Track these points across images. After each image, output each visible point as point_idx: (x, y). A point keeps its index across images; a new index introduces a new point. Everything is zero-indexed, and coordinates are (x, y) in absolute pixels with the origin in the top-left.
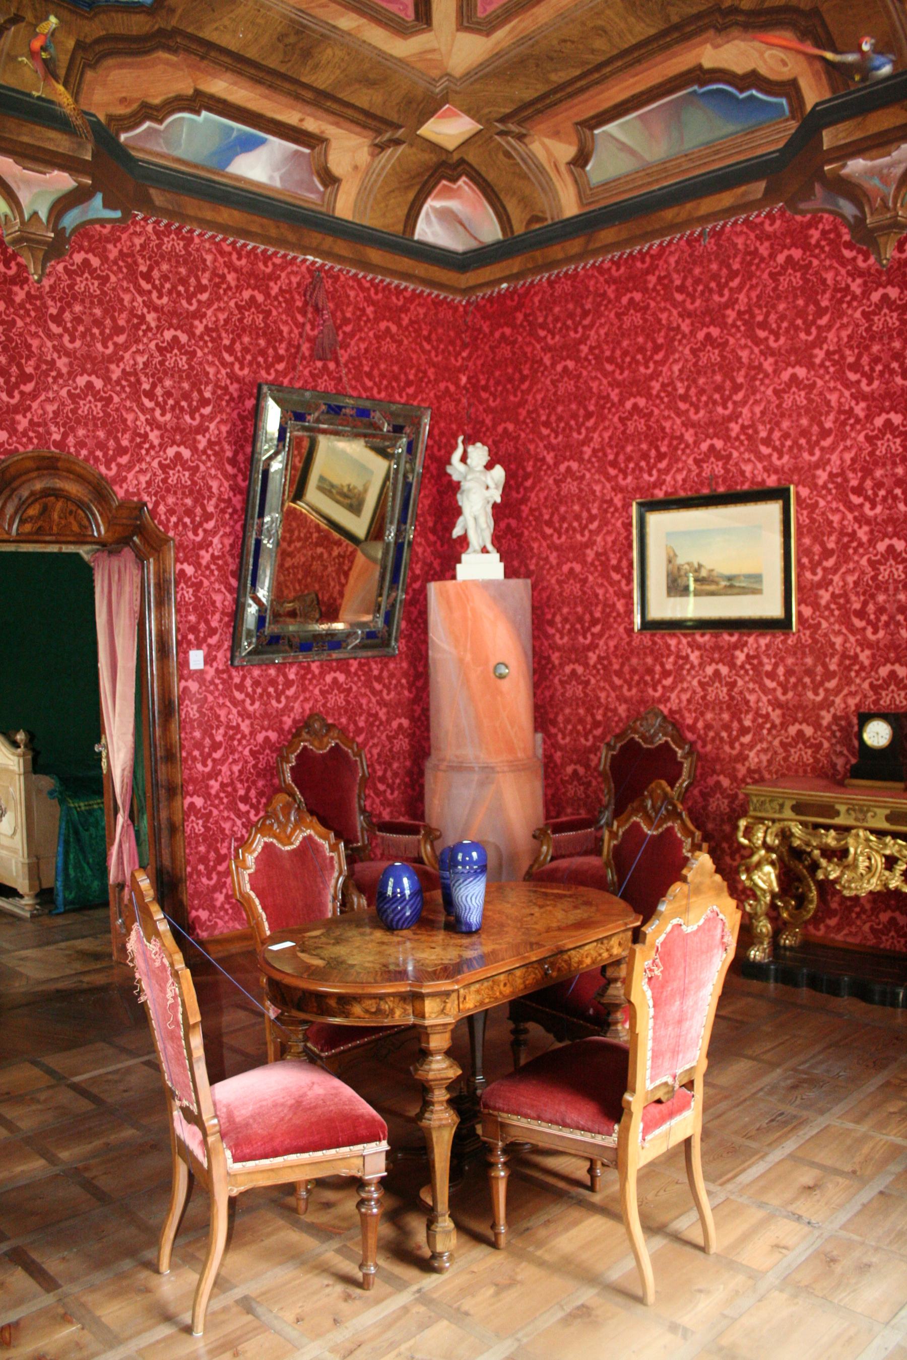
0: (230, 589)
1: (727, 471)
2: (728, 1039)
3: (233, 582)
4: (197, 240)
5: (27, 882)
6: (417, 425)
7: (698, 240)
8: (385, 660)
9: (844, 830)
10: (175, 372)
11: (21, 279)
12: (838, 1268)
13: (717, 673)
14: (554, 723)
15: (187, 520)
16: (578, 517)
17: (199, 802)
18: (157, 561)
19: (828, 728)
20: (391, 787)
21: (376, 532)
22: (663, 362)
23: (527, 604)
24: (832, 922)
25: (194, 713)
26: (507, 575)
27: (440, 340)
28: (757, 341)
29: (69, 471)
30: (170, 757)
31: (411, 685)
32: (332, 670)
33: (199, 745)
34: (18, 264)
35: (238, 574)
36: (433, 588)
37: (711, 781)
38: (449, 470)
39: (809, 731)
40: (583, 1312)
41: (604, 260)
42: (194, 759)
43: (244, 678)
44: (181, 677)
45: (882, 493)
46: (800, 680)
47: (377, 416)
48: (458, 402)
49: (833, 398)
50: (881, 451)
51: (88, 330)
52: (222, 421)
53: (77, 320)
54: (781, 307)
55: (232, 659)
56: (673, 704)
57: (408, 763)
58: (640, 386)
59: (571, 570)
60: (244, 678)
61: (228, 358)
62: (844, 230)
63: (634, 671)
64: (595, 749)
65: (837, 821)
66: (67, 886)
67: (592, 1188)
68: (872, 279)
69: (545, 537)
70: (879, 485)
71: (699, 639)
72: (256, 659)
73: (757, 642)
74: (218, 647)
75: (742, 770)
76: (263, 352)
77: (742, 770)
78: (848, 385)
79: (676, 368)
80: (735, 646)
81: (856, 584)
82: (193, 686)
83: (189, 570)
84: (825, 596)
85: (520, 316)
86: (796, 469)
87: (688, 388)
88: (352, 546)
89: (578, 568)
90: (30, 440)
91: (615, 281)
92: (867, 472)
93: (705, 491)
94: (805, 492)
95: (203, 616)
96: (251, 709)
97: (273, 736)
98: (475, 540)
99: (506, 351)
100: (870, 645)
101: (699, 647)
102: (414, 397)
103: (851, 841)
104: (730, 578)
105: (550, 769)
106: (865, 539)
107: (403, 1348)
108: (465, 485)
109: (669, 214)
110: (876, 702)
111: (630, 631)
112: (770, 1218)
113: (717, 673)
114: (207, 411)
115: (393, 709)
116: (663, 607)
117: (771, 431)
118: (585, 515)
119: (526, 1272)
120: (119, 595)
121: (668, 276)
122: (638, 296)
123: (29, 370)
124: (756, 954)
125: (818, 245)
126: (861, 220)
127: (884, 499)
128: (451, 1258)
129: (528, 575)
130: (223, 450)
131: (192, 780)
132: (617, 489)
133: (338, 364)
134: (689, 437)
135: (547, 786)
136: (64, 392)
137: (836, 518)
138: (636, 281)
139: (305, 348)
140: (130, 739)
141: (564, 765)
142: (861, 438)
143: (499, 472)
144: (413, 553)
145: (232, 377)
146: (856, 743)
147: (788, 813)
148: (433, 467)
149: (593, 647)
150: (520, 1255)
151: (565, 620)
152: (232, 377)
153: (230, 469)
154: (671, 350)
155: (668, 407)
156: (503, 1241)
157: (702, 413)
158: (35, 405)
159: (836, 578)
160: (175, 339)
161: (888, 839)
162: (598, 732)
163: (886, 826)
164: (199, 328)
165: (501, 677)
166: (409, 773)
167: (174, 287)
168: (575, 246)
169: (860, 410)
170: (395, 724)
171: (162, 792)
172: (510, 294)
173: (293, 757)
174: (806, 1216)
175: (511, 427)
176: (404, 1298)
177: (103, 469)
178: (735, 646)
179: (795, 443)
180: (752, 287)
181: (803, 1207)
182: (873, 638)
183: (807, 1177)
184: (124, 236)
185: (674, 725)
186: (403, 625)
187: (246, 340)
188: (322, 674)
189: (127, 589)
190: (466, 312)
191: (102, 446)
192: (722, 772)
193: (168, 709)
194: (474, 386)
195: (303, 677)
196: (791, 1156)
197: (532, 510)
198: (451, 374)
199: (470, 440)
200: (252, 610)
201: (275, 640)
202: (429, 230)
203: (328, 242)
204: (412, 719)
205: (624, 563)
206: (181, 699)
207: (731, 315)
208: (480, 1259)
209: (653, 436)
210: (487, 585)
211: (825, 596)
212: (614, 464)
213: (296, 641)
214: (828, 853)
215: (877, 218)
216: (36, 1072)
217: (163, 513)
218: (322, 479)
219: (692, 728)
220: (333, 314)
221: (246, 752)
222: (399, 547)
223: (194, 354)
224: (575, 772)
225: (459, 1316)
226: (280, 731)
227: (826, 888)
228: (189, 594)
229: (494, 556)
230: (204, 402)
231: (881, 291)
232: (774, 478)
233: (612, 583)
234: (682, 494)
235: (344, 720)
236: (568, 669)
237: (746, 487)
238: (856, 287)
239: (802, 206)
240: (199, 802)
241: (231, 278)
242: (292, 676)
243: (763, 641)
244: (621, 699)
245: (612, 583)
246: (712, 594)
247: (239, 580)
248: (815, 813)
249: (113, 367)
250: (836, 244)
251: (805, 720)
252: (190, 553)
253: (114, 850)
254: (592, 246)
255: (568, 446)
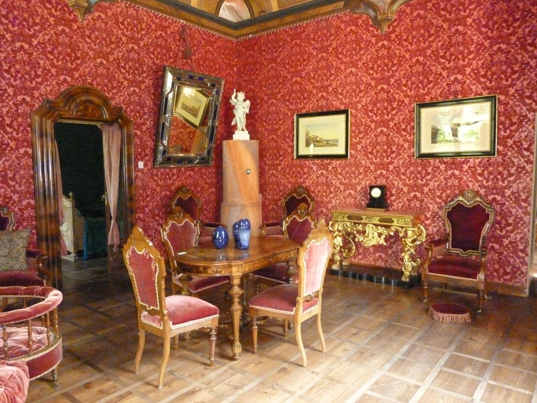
0: (153, 140)
1: (327, 104)
2: (328, 291)
3: (154, 137)
4: (141, 11)
5: (73, 248)
6: (220, 84)
7: (320, 22)
8: (208, 167)
9: (366, 224)
10: (133, 60)
11: (75, 21)
12: (365, 355)
13: (322, 173)
14: (266, 191)
15: (138, 114)
16: (275, 119)
17: (141, 216)
18: (127, 128)
19: (360, 191)
20: (209, 212)
21: (203, 123)
22: (306, 65)
23: (257, 149)
24: (360, 257)
25: (140, 184)
26: (252, 138)
27: (227, 54)
28: (339, 59)
29: (93, 93)
30: (131, 199)
31: (216, 177)
32: (189, 170)
33: (141, 195)
34: (74, 15)
35: (156, 134)
36: (225, 142)
37: (319, 210)
38: (230, 101)
39: (353, 192)
40: (284, 369)
41: (287, 28)
42: (140, 200)
43: (158, 172)
44: (136, 171)
45: (380, 112)
46: (350, 175)
47: (206, 80)
48: (233, 77)
49: (364, 79)
50: (380, 97)
51: (101, 42)
52: (150, 79)
53: (97, 38)
54: (348, 47)
55: (154, 165)
56: (307, 184)
57: (215, 204)
58: (298, 73)
59: (273, 138)
60: (158, 172)
61: (152, 56)
62: (370, 20)
63: (294, 173)
64: (279, 200)
65: (362, 221)
66: (88, 248)
67: (284, 336)
68: (379, 38)
69: (264, 126)
70: (379, 109)
71: (316, 161)
72: (162, 166)
73: (336, 163)
74: (149, 160)
75: (330, 206)
76: (165, 55)
77: (330, 206)
78: (369, 74)
79: (311, 67)
80: (328, 164)
81: (370, 143)
82: (140, 174)
83: (138, 133)
84: (359, 147)
85: (256, 47)
86: (351, 103)
87: (315, 75)
88: (194, 129)
89: (275, 137)
90: (79, 81)
91: (290, 35)
92: (375, 105)
93: (320, 111)
94: (353, 111)
95: (143, 149)
96: (160, 183)
97: (168, 193)
98: (239, 126)
99: (251, 60)
100: (374, 164)
101: (316, 164)
102: (218, 74)
103: (367, 228)
104: (327, 141)
105: (264, 206)
106: (373, 128)
107: (226, 382)
108: (236, 107)
109: (311, 12)
110: (376, 183)
111: (293, 159)
112: (343, 342)
113: (322, 173)
114: (145, 75)
115: (210, 185)
116: (303, 151)
117: (343, 90)
118: (278, 118)
119: (264, 359)
120: (113, 140)
121: (309, 34)
122: (298, 41)
123: (79, 55)
124: (335, 267)
125: (361, 25)
126: (376, 17)
127: (380, 114)
128: (240, 355)
129: (258, 139)
130: (150, 90)
131: (139, 208)
132: (289, 109)
133: (191, 61)
134: (314, 92)
135: (263, 213)
136: (92, 65)
137: (364, 120)
138: (297, 36)
139: (180, 54)
140: (116, 193)
141: (269, 206)
142: (373, 93)
143: (248, 102)
144: (217, 130)
145: (154, 63)
146: (369, 196)
147: (346, 219)
148: (224, 101)
149: (279, 164)
150: (262, 355)
151: (270, 155)
152: (154, 63)
153: (153, 96)
154: (309, 61)
155: (435, 61)
156: (256, 350)
157: (319, 84)
158: (81, 69)
159: (363, 141)
160: (133, 48)
161: (379, 227)
162: (281, 194)
163: (379, 223)
164: (142, 44)
165: (248, 174)
166: (215, 207)
167: (132, 28)
168: (276, 22)
169: (373, 83)
170: (210, 191)
171: (129, 211)
172: (253, 39)
173: (176, 200)
174: (354, 342)
175: (252, 87)
176: (225, 368)
177: (107, 94)
178: (328, 164)
179: (351, 94)
180: (338, 40)
181: (353, 339)
182: (375, 161)
183: (354, 331)
184: (114, 7)
185: (307, 190)
186: (214, 156)
187: (159, 50)
188: (185, 172)
189: (115, 138)
190: (237, 45)
191: (106, 85)
192: (323, 207)
193: (131, 183)
194: (239, 72)
195: (179, 173)
196: (349, 325)
197: (259, 117)
198: (230, 67)
199: (238, 91)
200: (161, 148)
201: (169, 159)
202: (224, 14)
203: (188, 15)
204: (217, 189)
205: (291, 136)
206: (135, 179)
207: (330, 49)
208: (249, 357)
209: (302, 91)
210: (244, 142)
211: (359, 147)
212: (288, 101)
213: (176, 160)
214: (359, 232)
215: (382, 17)
216: (85, 309)
217: (129, 112)
218: (183, 104)
219: (313, 192)
220: (190, 42)
221: (158, 198)
222: (213, 128)
223: (140, 54)
224: (273, 208)
225: (244, 372)
226: (170, 191)
227: (358, 245)
228: (138, 141)
229: (246, 132)
230: (144, 72)
231: (382, 42)
232: (343, 106)
233: (287, 142)
234: (312, 112)
235: (193, 188)
236: (271, 172)
237: (334, 109)
238: (373, 40)
239: (357, 11)
240: (141, 216)
241: (153, 26)
242: (175, 172)
243: (338, 162)
244: (290, 182)
245: (287, 142)
246: (321, 146)
247: (156, 137)
248: (355, 219)
249: (110, 56)
250: (367, 25)
251: (352, 189)
252: (139, 127)
253: (110, 233)
254: (282, 23)
255: (272, 94)
